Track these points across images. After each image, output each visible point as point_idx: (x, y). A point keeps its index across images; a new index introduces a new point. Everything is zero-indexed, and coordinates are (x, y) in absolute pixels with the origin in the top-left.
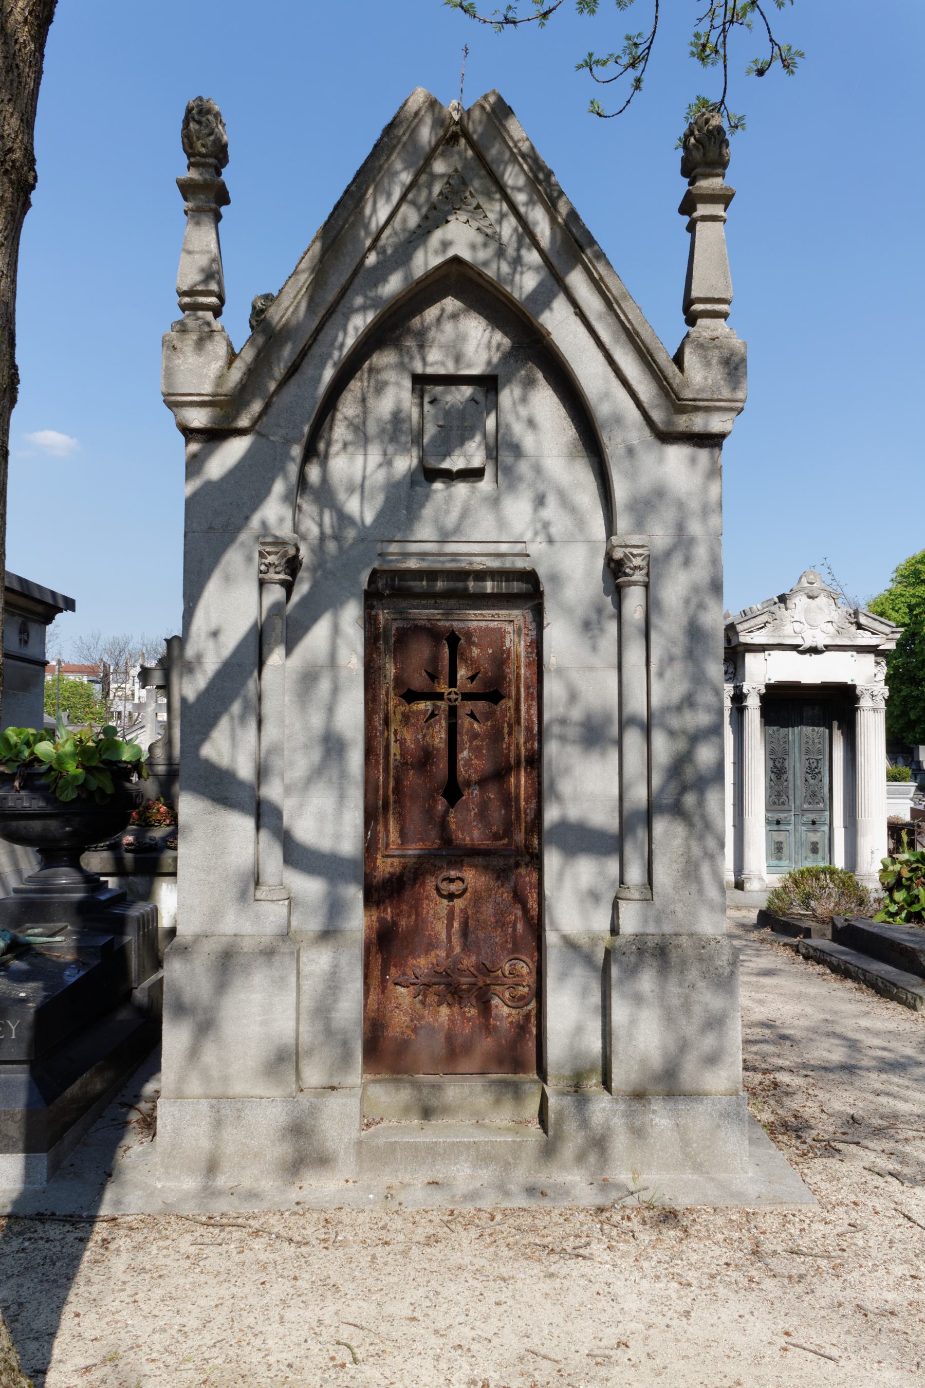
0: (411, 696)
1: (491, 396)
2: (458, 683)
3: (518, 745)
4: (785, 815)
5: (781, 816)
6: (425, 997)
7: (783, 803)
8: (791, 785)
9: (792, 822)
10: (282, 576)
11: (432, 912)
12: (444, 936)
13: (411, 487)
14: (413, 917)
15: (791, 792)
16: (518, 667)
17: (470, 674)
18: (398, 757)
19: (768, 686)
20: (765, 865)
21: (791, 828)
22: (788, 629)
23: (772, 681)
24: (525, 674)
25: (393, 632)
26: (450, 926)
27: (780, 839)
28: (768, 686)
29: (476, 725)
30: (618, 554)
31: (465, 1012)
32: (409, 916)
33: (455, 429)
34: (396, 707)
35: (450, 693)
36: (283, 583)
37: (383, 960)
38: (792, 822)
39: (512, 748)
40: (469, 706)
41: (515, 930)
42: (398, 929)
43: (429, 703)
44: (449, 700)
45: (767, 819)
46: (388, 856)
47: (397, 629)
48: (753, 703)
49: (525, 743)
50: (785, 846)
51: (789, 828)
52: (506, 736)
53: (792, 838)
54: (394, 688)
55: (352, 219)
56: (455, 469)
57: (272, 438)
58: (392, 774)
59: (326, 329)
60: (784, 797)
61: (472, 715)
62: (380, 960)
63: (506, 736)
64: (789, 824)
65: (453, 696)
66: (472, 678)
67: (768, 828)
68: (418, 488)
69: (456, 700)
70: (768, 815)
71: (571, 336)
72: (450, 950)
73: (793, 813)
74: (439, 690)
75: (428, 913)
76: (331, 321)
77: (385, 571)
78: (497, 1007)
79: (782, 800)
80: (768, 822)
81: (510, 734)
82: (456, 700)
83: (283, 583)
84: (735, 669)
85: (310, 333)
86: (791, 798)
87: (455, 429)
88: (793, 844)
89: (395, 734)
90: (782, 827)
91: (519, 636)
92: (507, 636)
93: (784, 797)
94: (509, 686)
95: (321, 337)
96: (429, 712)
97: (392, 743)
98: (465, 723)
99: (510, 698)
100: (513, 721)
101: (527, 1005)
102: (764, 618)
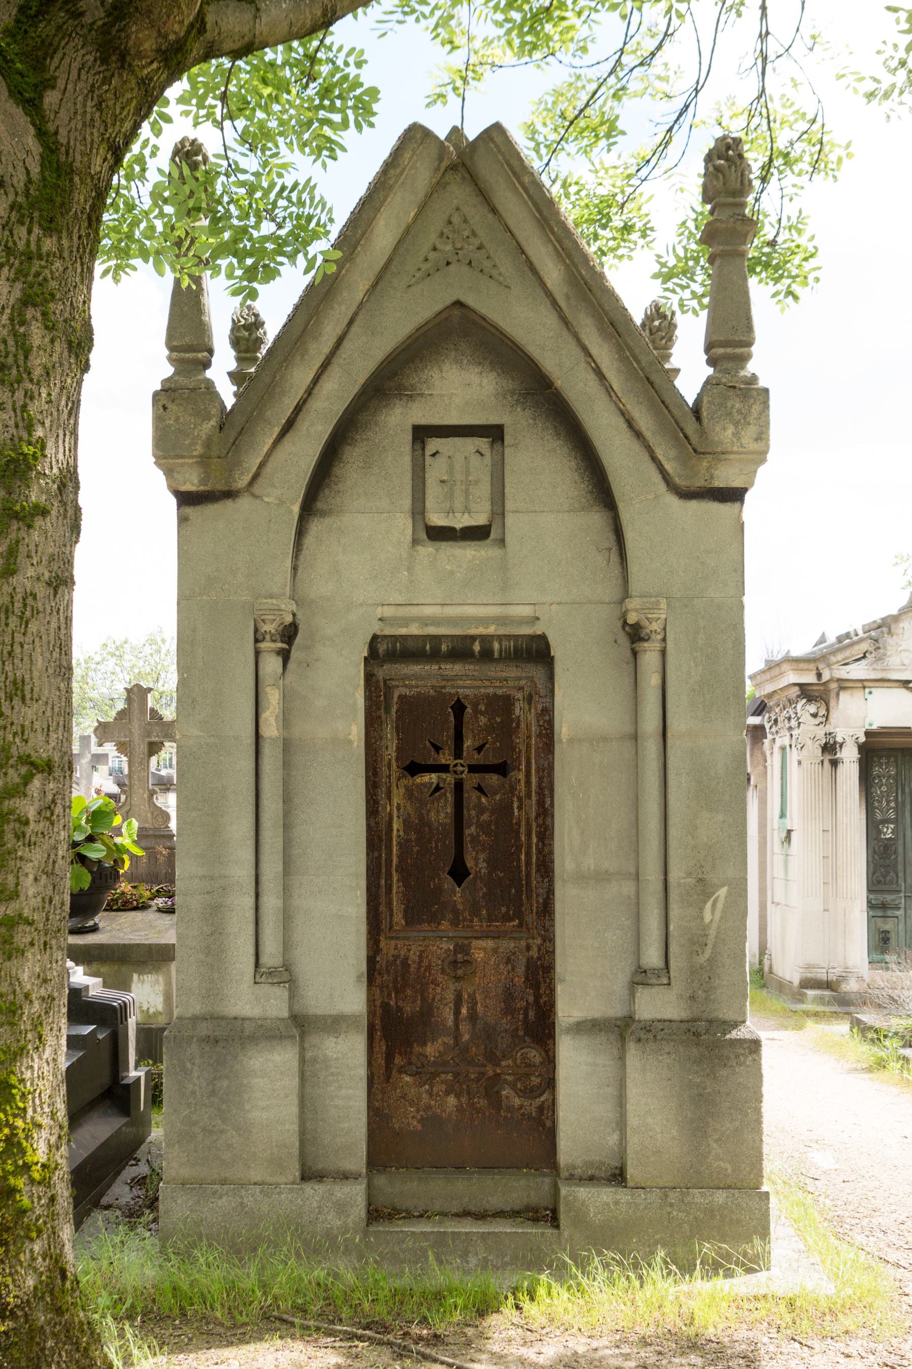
0: (414, 769)
1: (497, 446)
2: (465, 754)
3: (528, 819)
4: (893, 897)
5: (889, 898)
6: (432, 1087)
7: (891, 882)
8: (900, 859)
9: (902, 905)
10: (280, 645)
11: (438, 997)
12: (450, 1022)
13: (413, 546)
14: (419, 1002)
15: (900, 867)
16: (529, 737)
17: (477, 744)
18: (401, 833)
19: (868, 734)
20: (867, 960)
21: (900, 913)
22: (894, 660)
23: (874, 727)
24: (536, 744)
25: (395, 700)
26: (457, 1012)
27: (887, 927)
28: (868, 734)
29: (483, 800)
30: (632, 618)
31: (473, 1103)
32: (414, 1001)
33: (459, 483)
34: (399, 779)
35: (455, 765)
36: (280, 652)
37: (387, 1046)
38: (902, 905)
39: (523, 823)
40: (475, 778)
41: (526, 1015)
42: (402, 1014)
43: (434, 776)
44: (455, 772)
45: (869, 902)
46: (391, 938)
47: (400, 697)
48: (850, 755)
49: (536, 818)
50: (893, 936)
51: (898, 913)
52: (516, 811)
53: (901, 926)
54: (397, 760)
55: (348, 265)
56: (458, 526)
57: (266, 499)
58: (187, 355)
59: (321, 382)
60: (892, 874)
61: (479, 789)
62: (384, 1048)
63: (516, 811)
64: (899, 908)
65: (460, 769)
66: (479, 749)
67: (871, 913)
68: (419, 548)
69: (462, 773)
70: (871, 896)
71: (582, 384)
72: (457, 1036)
73: (902, 895)
74: (443, 762)
75: (433, 999)
76: (327, 374)
77: (385, 636)
78: (507, 1097)
79: (888, 878)
80: (871, 906)
81: (520, 808)
82: (462, 773)
83: (280, 652)
84: (828, 710)
85: (304, 388)
86: (901, 874)
87: (459, 483)
88: (902, 934)
89: (398, 809)
90: (890, 913)
91: (530, 704)
92: (517, 704)
93: (892, 874)
94: (519, 757)
95: (315, 391)
96: (434, 786)
97: (395, 818)
98: (471, 797)
99: (519, 770)
100: (523, 794)
101: (541, 1095)
102: (864, 646)
